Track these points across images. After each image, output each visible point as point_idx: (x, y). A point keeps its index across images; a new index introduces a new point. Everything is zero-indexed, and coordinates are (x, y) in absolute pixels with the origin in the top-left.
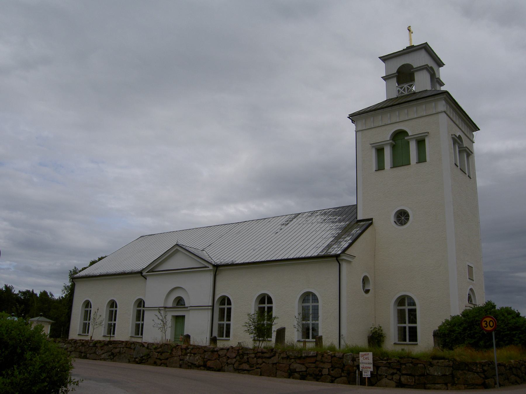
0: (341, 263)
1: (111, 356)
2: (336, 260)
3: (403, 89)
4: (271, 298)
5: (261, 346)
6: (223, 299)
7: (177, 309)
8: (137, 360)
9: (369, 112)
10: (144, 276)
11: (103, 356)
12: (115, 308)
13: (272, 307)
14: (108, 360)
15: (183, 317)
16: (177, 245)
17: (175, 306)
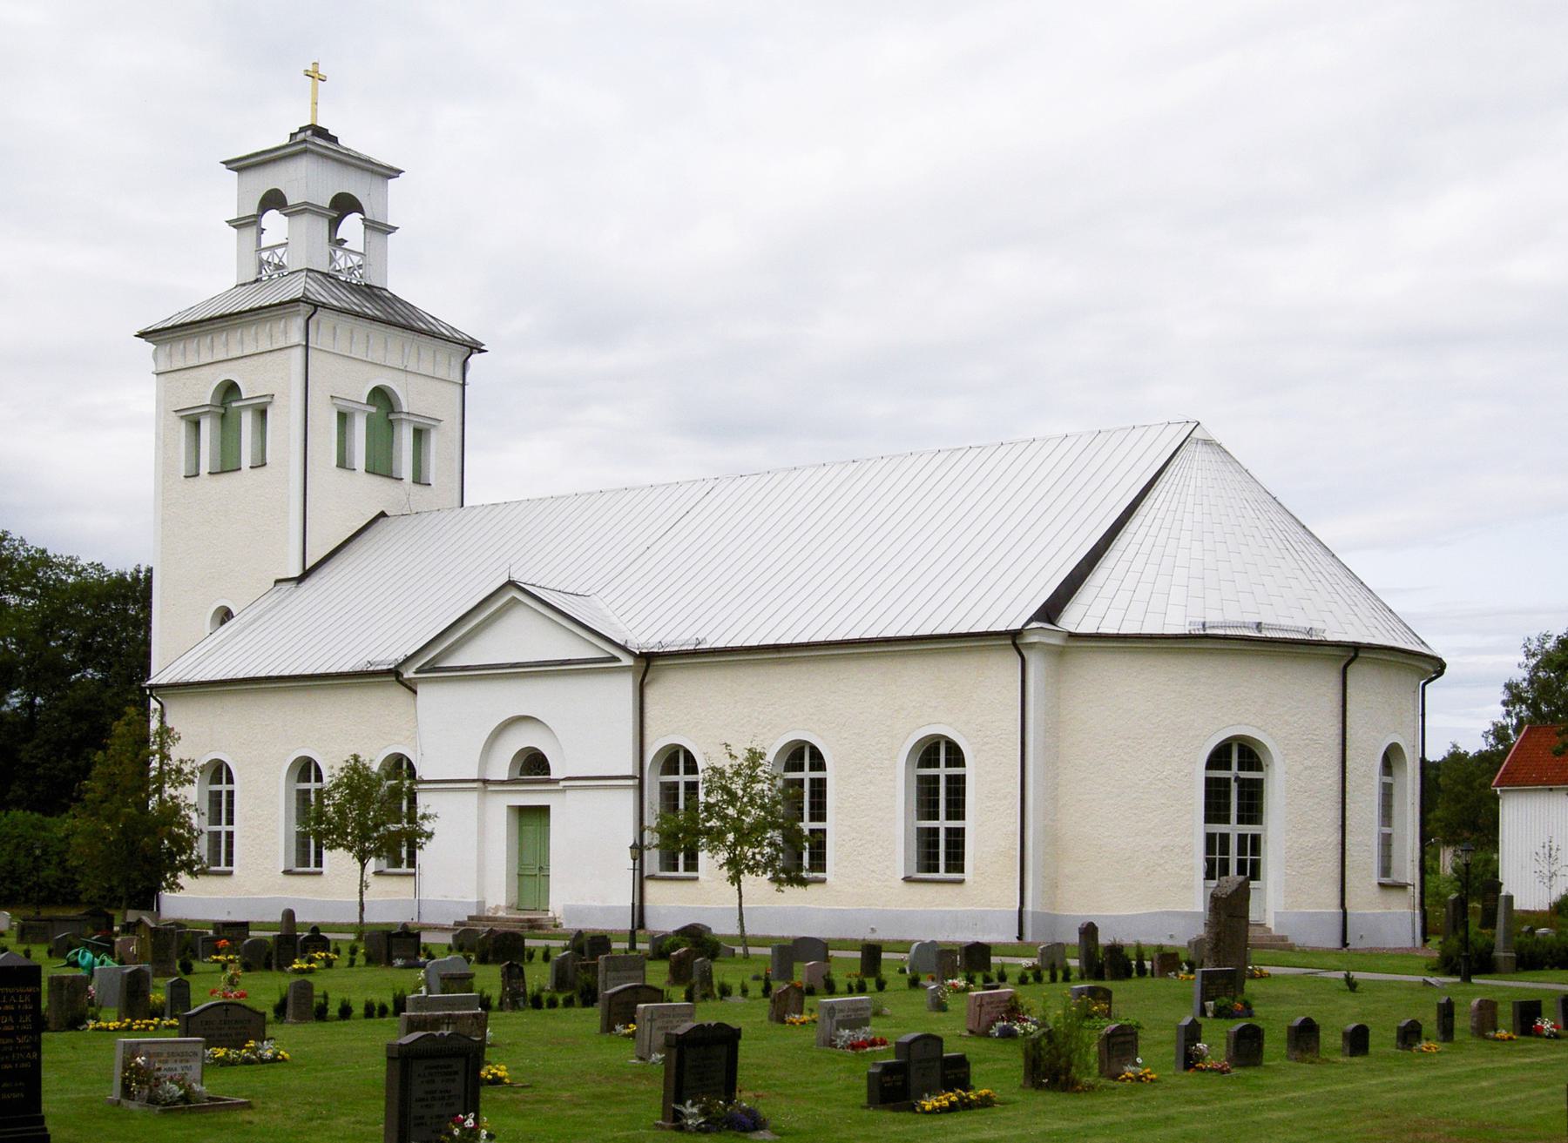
0: (1025, 653)
2: (1012, 647)
4: (960, 748)
6: (399, 760)
10: (407, 682)
12: (227, 783)
13: (825, 779)
15: (544, 811)
16: (511, 584)
17: (517, 775)
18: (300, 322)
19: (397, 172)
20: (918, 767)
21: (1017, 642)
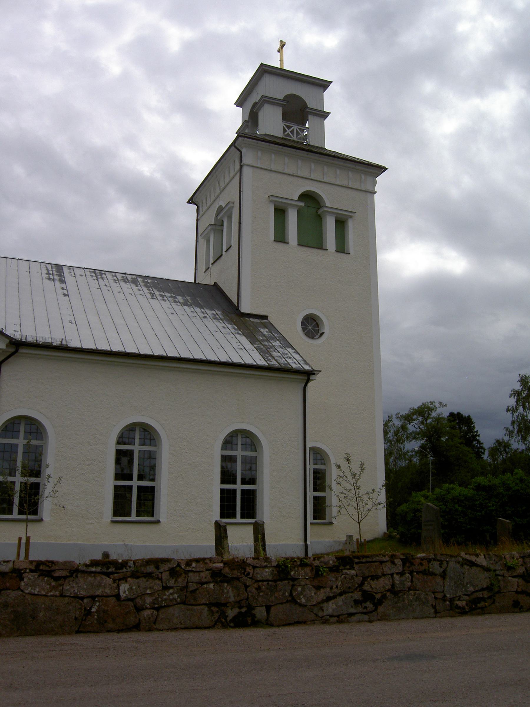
1: (364, 605)
5: (361, 540)
8: (460, 603)
11: (331, 607)
14: (354, 618)
19: (332, 82)
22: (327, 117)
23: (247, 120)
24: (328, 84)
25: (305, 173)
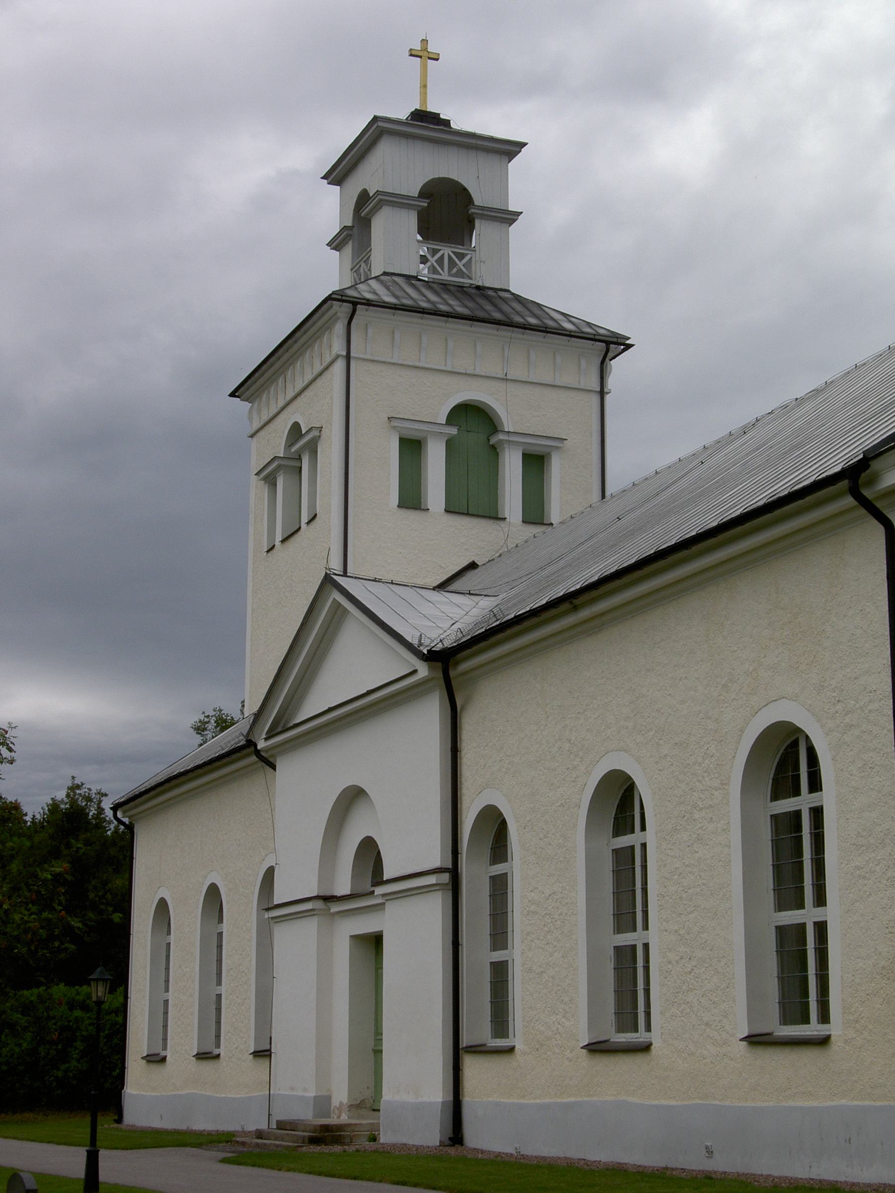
3: (437, 267)
7: (420, 891)
9: (431, 314)
18: (339, 328)
19: (525, 144)
20: (771, 801)
21: (867, 493)
22: (514, 221)
23: (350, 224)
24: (517, 149)
25: (463, 362)
